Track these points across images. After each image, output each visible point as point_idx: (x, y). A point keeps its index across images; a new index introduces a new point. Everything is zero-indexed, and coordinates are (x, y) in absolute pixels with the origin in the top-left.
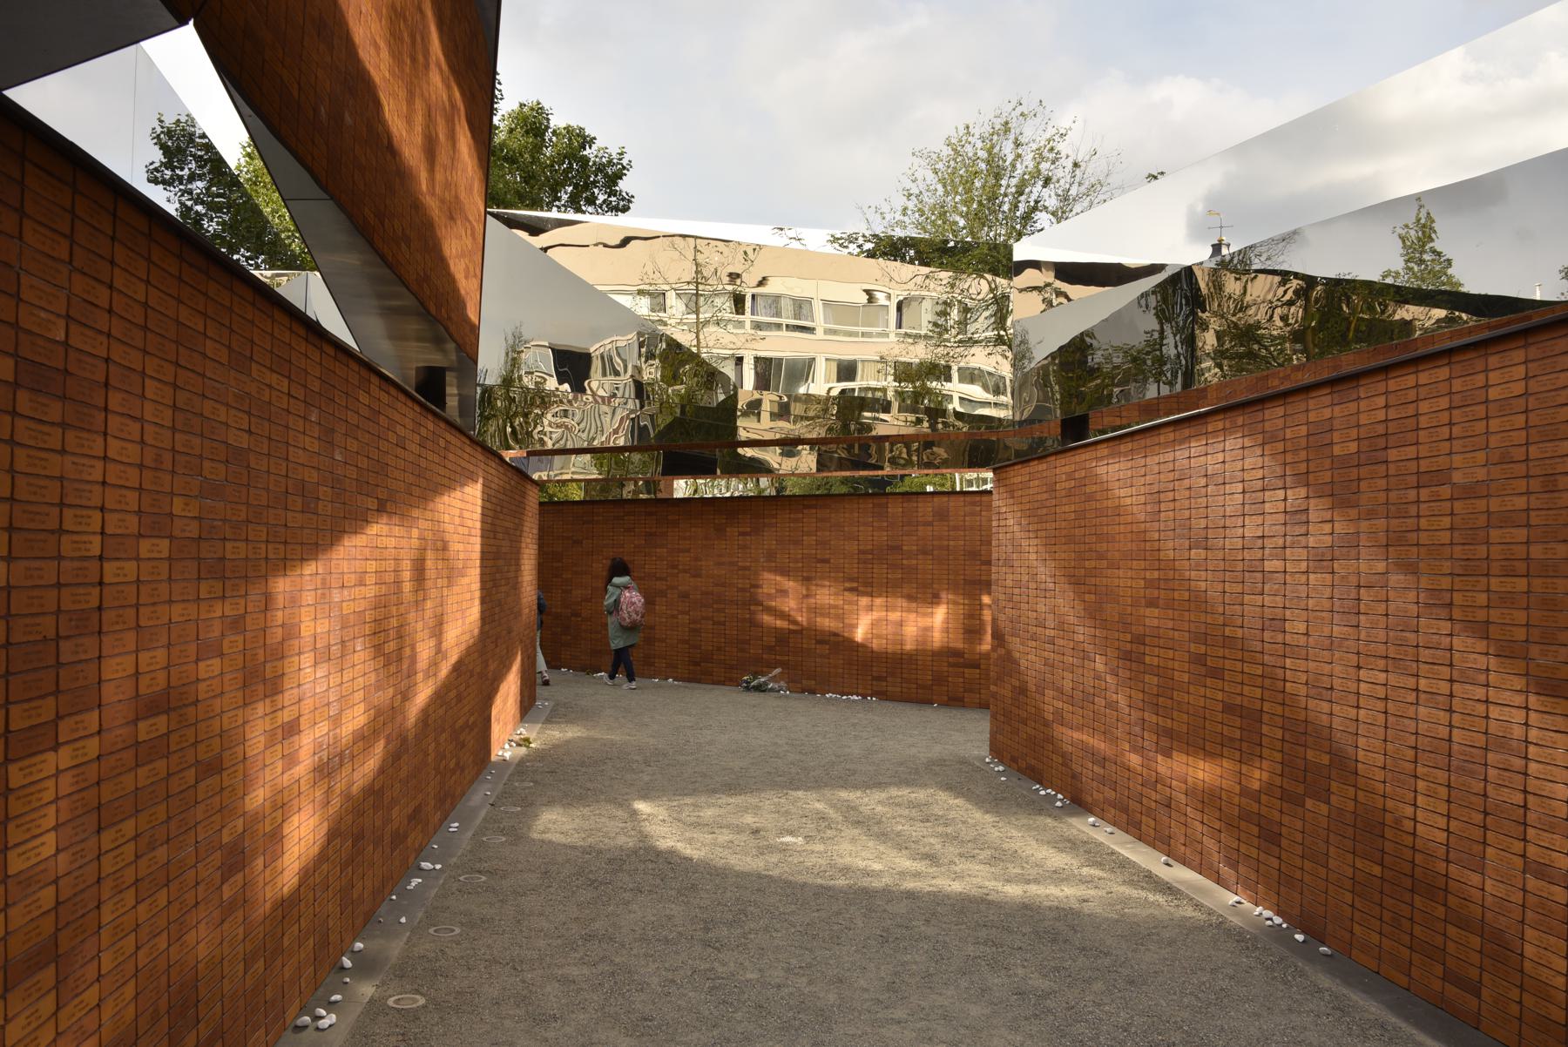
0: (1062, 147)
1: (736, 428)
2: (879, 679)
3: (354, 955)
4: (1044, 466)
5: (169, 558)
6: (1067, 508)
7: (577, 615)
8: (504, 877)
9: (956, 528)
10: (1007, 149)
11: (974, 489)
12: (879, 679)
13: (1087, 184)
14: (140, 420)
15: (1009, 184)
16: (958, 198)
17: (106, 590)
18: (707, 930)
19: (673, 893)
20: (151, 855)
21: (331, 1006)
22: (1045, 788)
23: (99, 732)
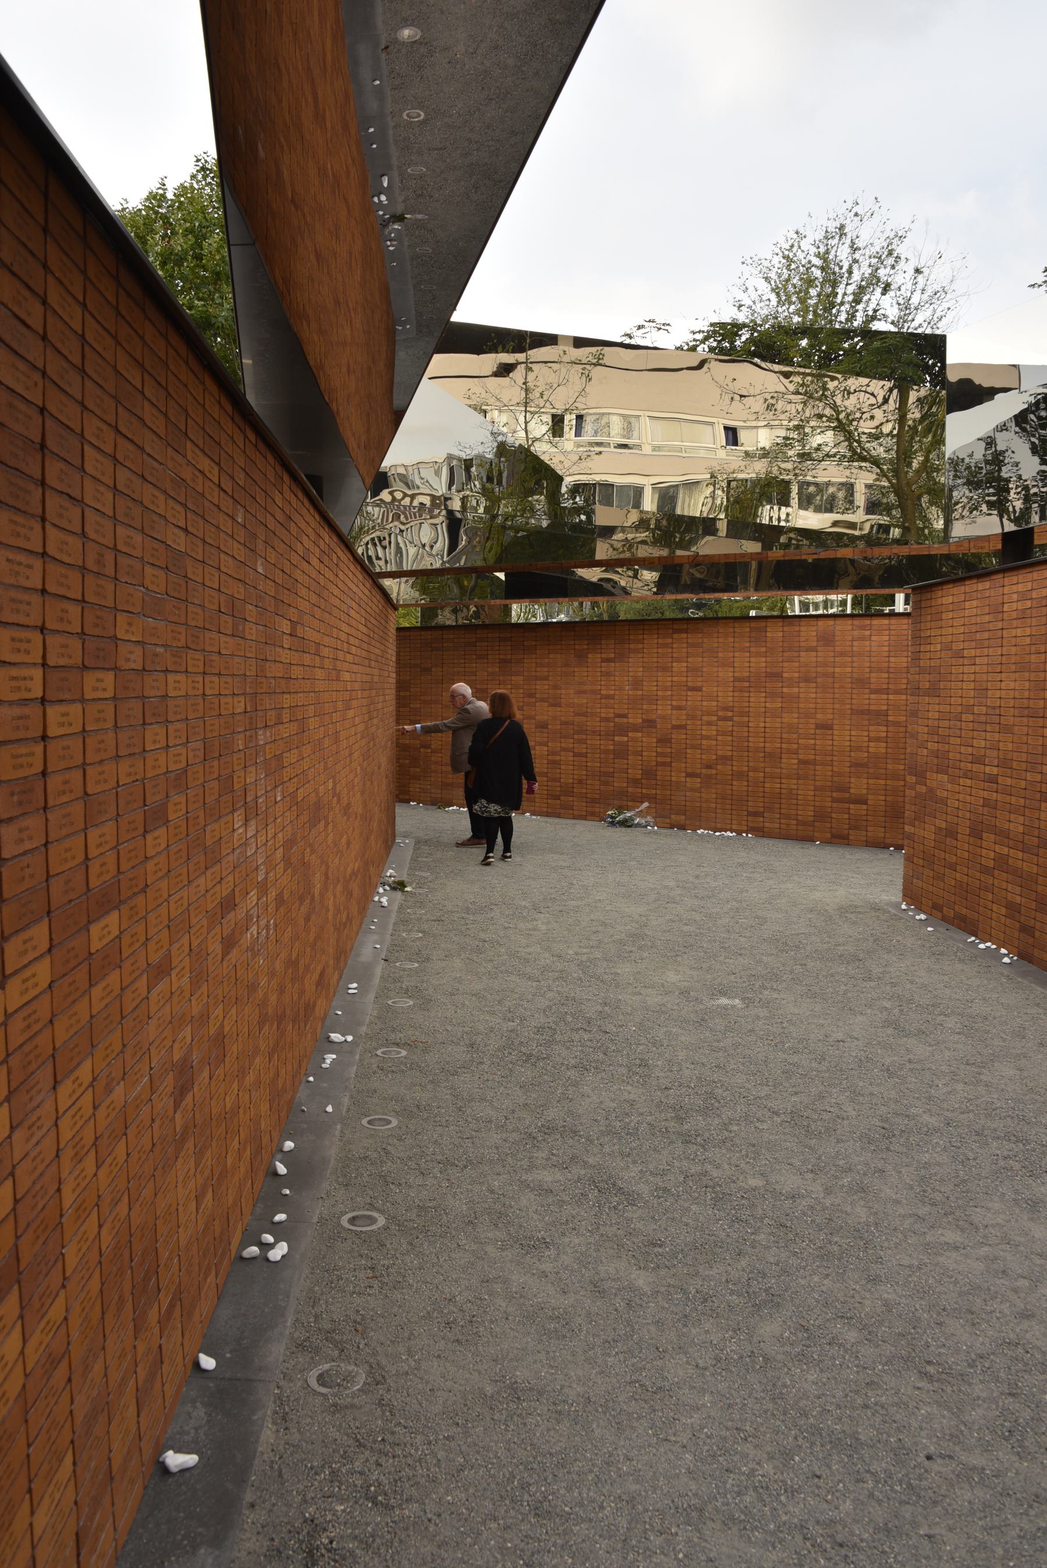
0: (901, 250)
1: (761, 524)
2: (756, 814)
3: (288, 1158)
4: (987, 585)
5: (114, 698)
6: (1019, 632)
7: (427, 746)
8: (425, 1051)
9: (842, 654)
10: (843, 254)
11: (820, 612)
12: (756, 814)
13: (929, 292)
14: (79, 502)
15: (845, 291)
16: (792, 308)
17: (52, 746)
18: (680, 1120)
19: (624, 1070)
20: (108, 1101)
21: (280, 1232)
22: (985, 942)
23: (50, 950)
